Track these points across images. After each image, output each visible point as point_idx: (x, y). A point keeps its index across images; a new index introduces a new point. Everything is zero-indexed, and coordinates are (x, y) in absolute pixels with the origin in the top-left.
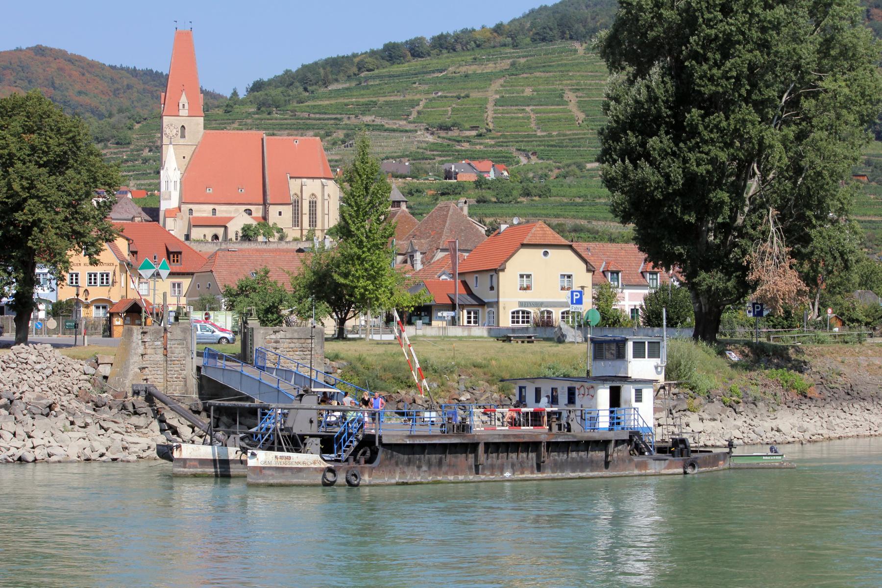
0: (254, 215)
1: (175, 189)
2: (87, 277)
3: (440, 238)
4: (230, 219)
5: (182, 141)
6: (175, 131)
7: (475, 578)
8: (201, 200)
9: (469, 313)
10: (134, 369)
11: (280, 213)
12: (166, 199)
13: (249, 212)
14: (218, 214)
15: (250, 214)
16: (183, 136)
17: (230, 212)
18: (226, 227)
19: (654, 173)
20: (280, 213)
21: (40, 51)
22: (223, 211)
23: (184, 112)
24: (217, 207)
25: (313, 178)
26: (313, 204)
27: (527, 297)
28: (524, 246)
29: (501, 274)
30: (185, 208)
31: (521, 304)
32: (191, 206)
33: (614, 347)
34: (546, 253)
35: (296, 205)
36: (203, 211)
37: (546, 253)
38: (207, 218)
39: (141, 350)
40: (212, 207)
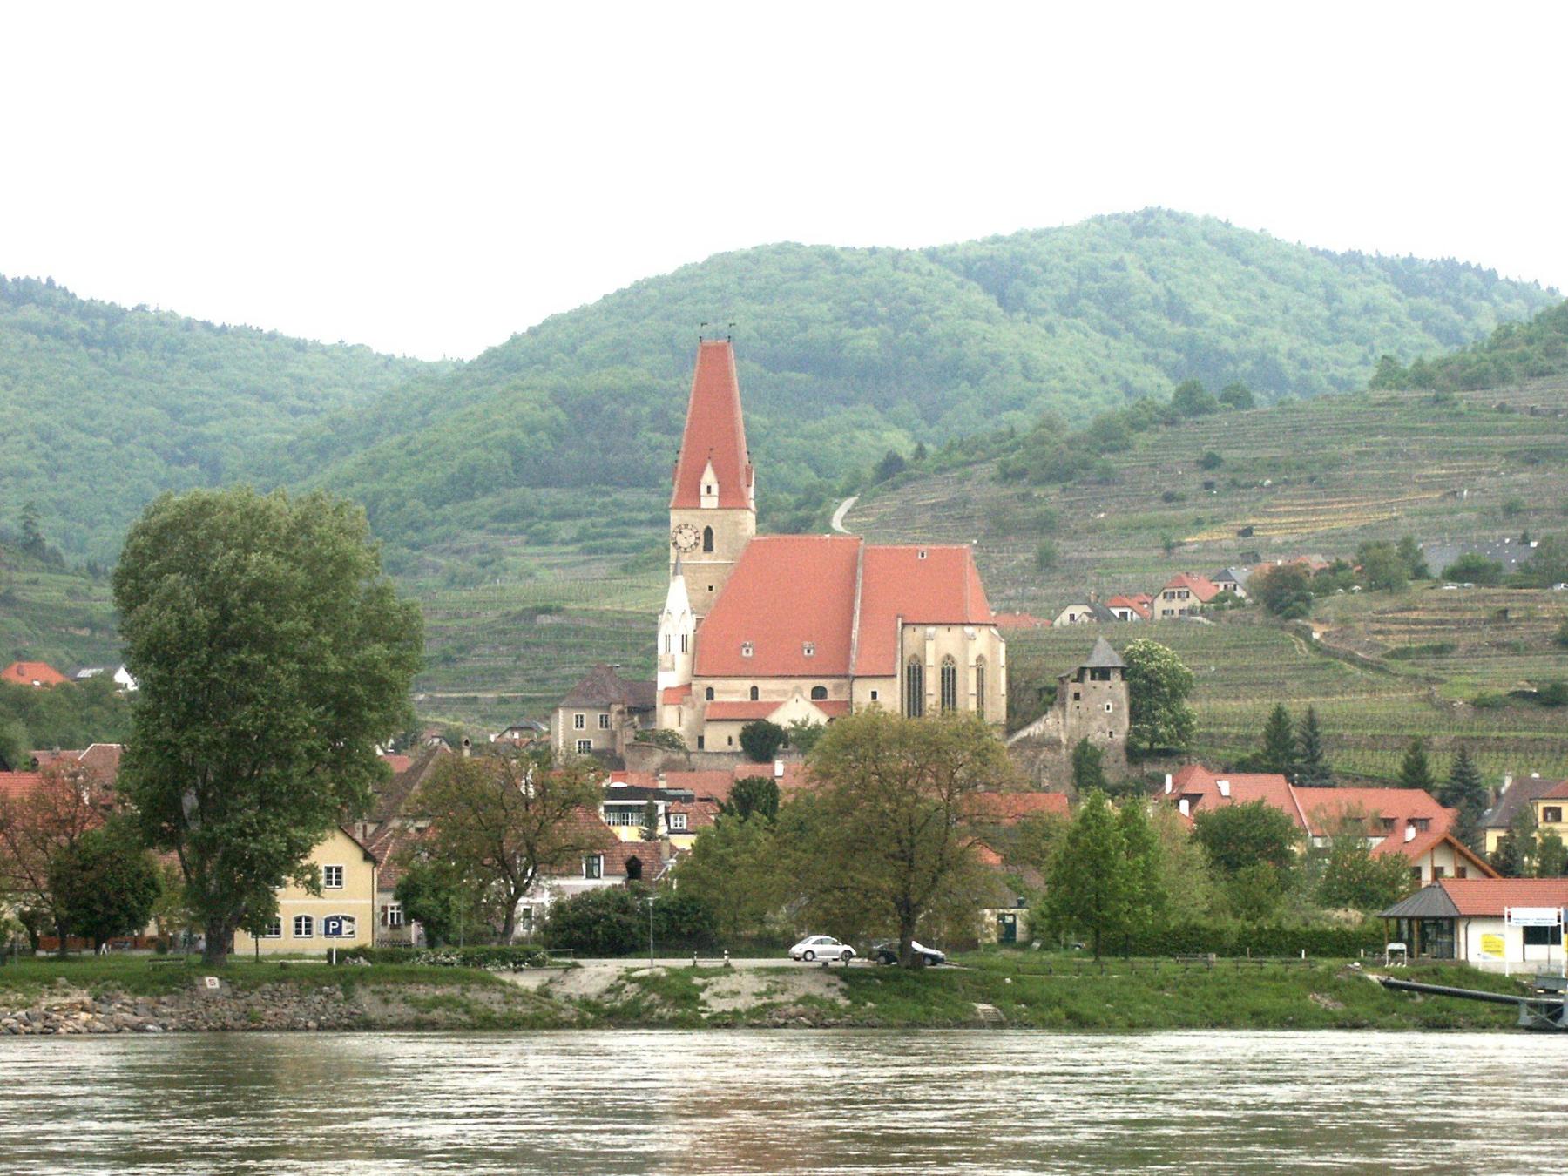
0: (831, 697)
1: (668, 637)
2: (292, 923)
5: (706, 559)
7: (1242, 1113)
11: (874, 694)
12: (666, 670)
14: (762, 698)
16: (708, 547)
19: (1306, 924)
21: (1145, 225)
23: (709, 502)
24: (761, 684)
26: (949, 677)
30: (699, 686)
32: (710, 683)
33: (1446, 923)
35: (915, 676)
38: (740, 704)
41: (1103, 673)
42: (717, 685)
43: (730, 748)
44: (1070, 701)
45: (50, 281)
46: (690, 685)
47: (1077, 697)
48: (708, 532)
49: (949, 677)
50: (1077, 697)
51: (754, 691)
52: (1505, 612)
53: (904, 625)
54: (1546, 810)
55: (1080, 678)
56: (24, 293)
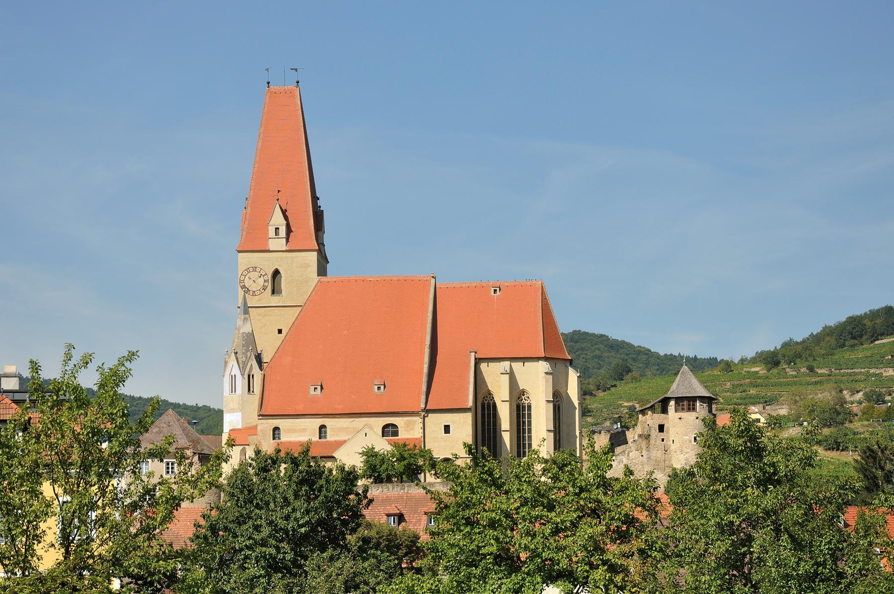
5: (275, 300)
8: (300, 409)
11: (447, 429)
14: (330, 437)
20: (447, 429)
24: (328, 422)
25: (524, 359)
40: (319, 422)
46: (255, 427)
48: (276, 273)
51: (322, 427)
53: (478, 361)
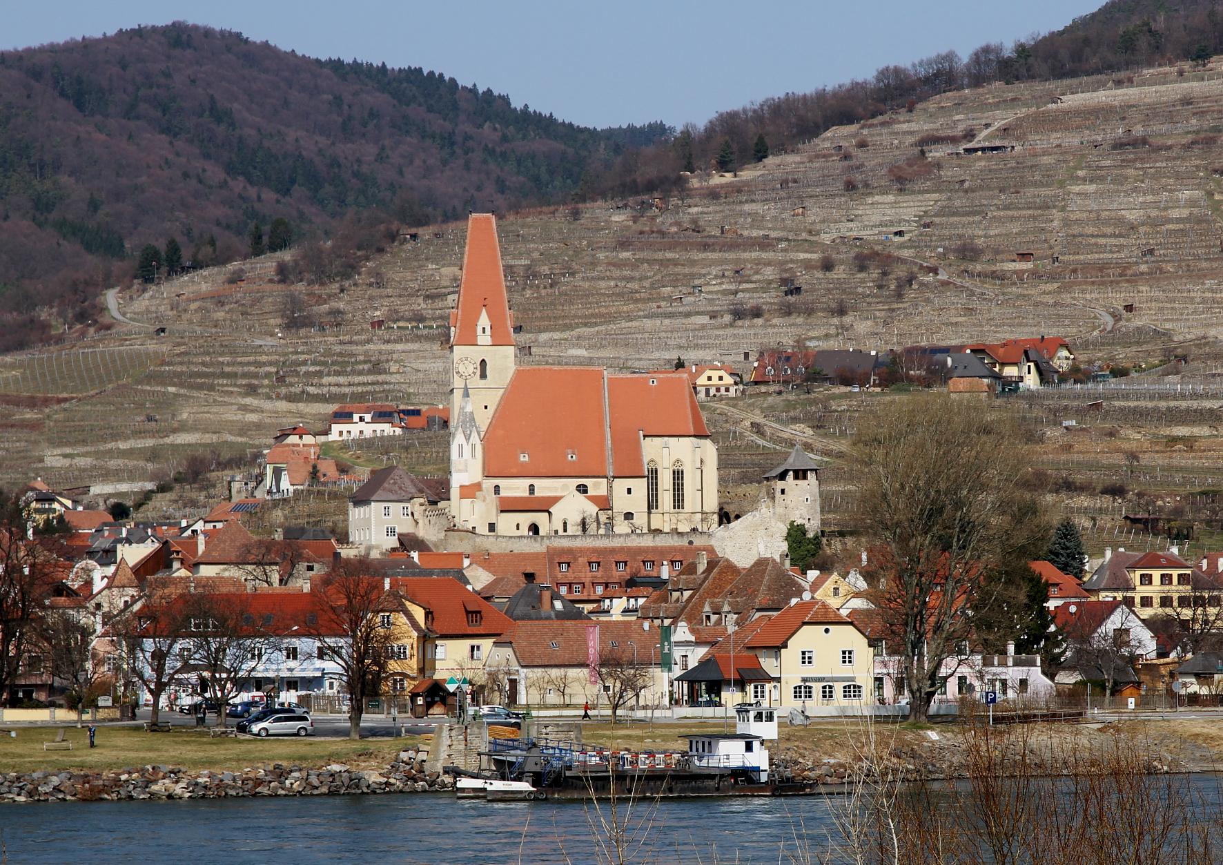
0: (591, 492)
1: (473, 456)
3: (756, 596)
4: (555, 500)
6: (471, 369)
9: (756, 687)
10: (444, 755)
11: (629, 491)
12: (459, 471)
13: (582, 489)
14: (537, 493)
15: (585, 492)
16: (483, 376)
17: (556, 489)
18: (550, 513)
20: (629, 491)
22: (545, 488)
26: (678, 476)
27: (808, 671)
28: (805, 624)
29: (783, 651)
30: (489, 484)
31: (804, 680)
34: (827, 631)
35: (652, 477)
36: (516, 488)
37: (827, 631)
38: (521, 498)
39: (449, 742)
41: (800, 474)
42: (501, 482)
43: (518, 533)
44: (778, 494)
45: (355, 61)
47: (783, 491)
49: (678, 476)
50: (783, 491)
51: (691, 542)
52: (1071, 446)
54: (1142, 576)
55: (782, 476)
56: (73, 77)
